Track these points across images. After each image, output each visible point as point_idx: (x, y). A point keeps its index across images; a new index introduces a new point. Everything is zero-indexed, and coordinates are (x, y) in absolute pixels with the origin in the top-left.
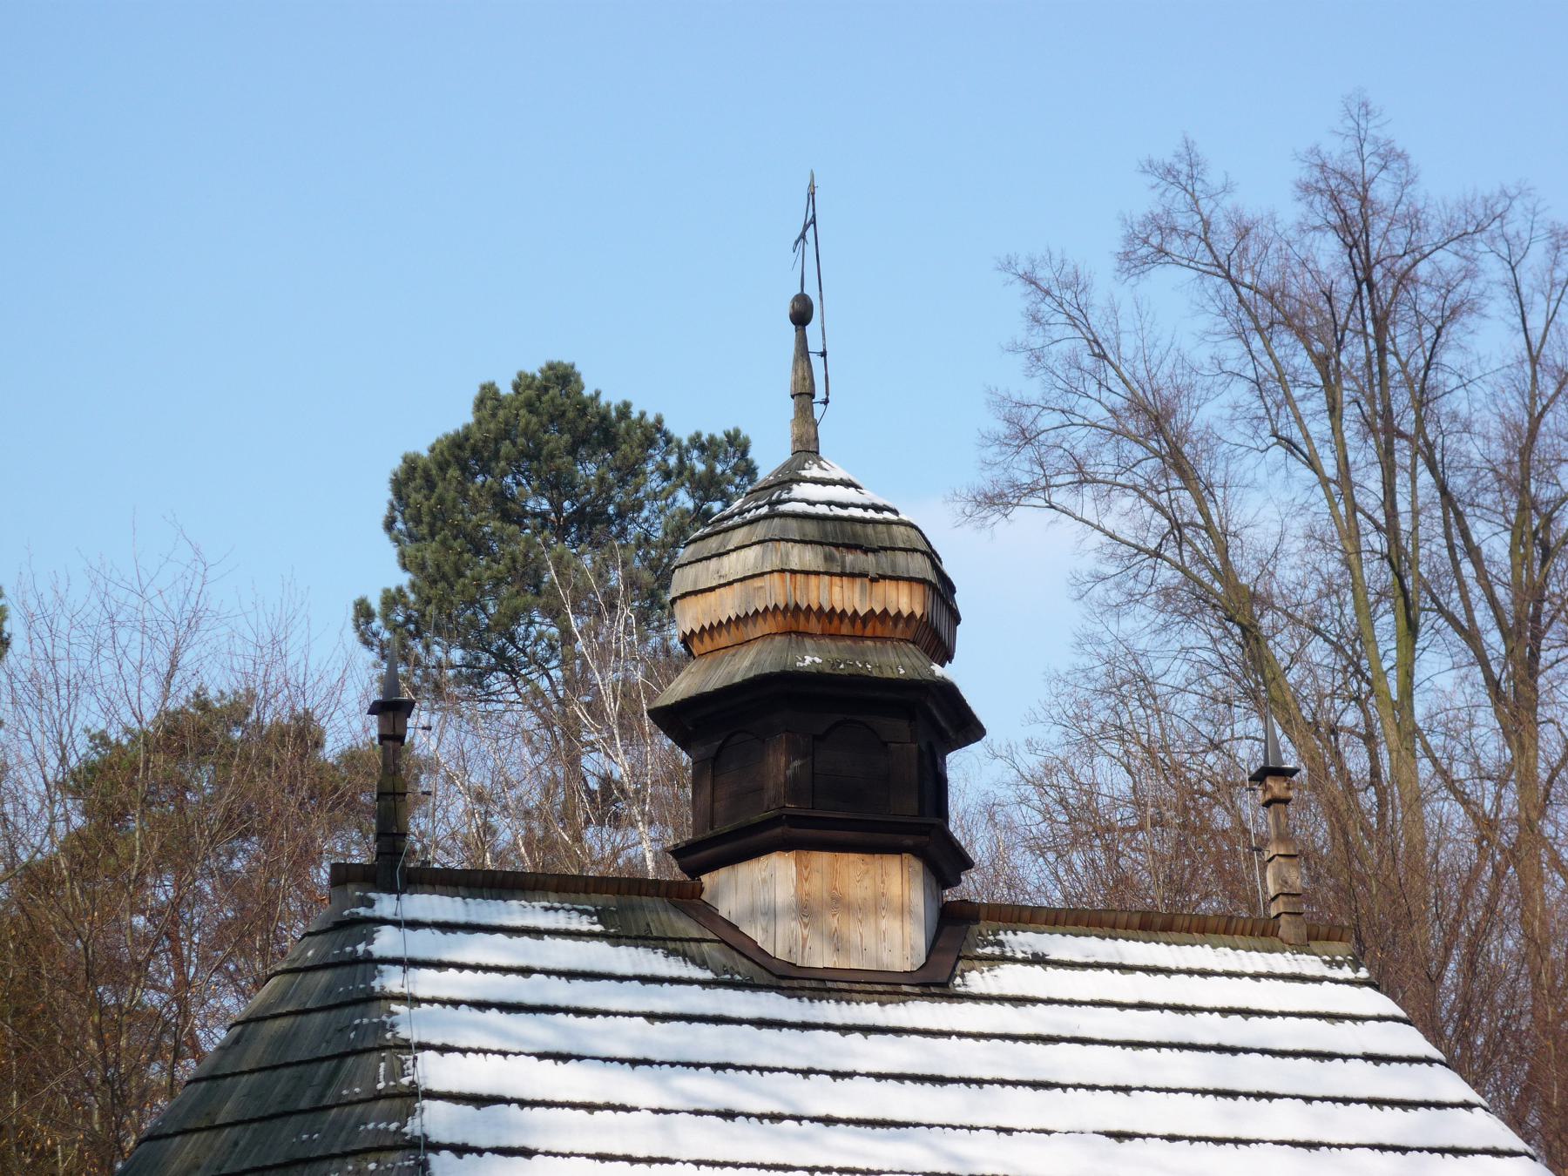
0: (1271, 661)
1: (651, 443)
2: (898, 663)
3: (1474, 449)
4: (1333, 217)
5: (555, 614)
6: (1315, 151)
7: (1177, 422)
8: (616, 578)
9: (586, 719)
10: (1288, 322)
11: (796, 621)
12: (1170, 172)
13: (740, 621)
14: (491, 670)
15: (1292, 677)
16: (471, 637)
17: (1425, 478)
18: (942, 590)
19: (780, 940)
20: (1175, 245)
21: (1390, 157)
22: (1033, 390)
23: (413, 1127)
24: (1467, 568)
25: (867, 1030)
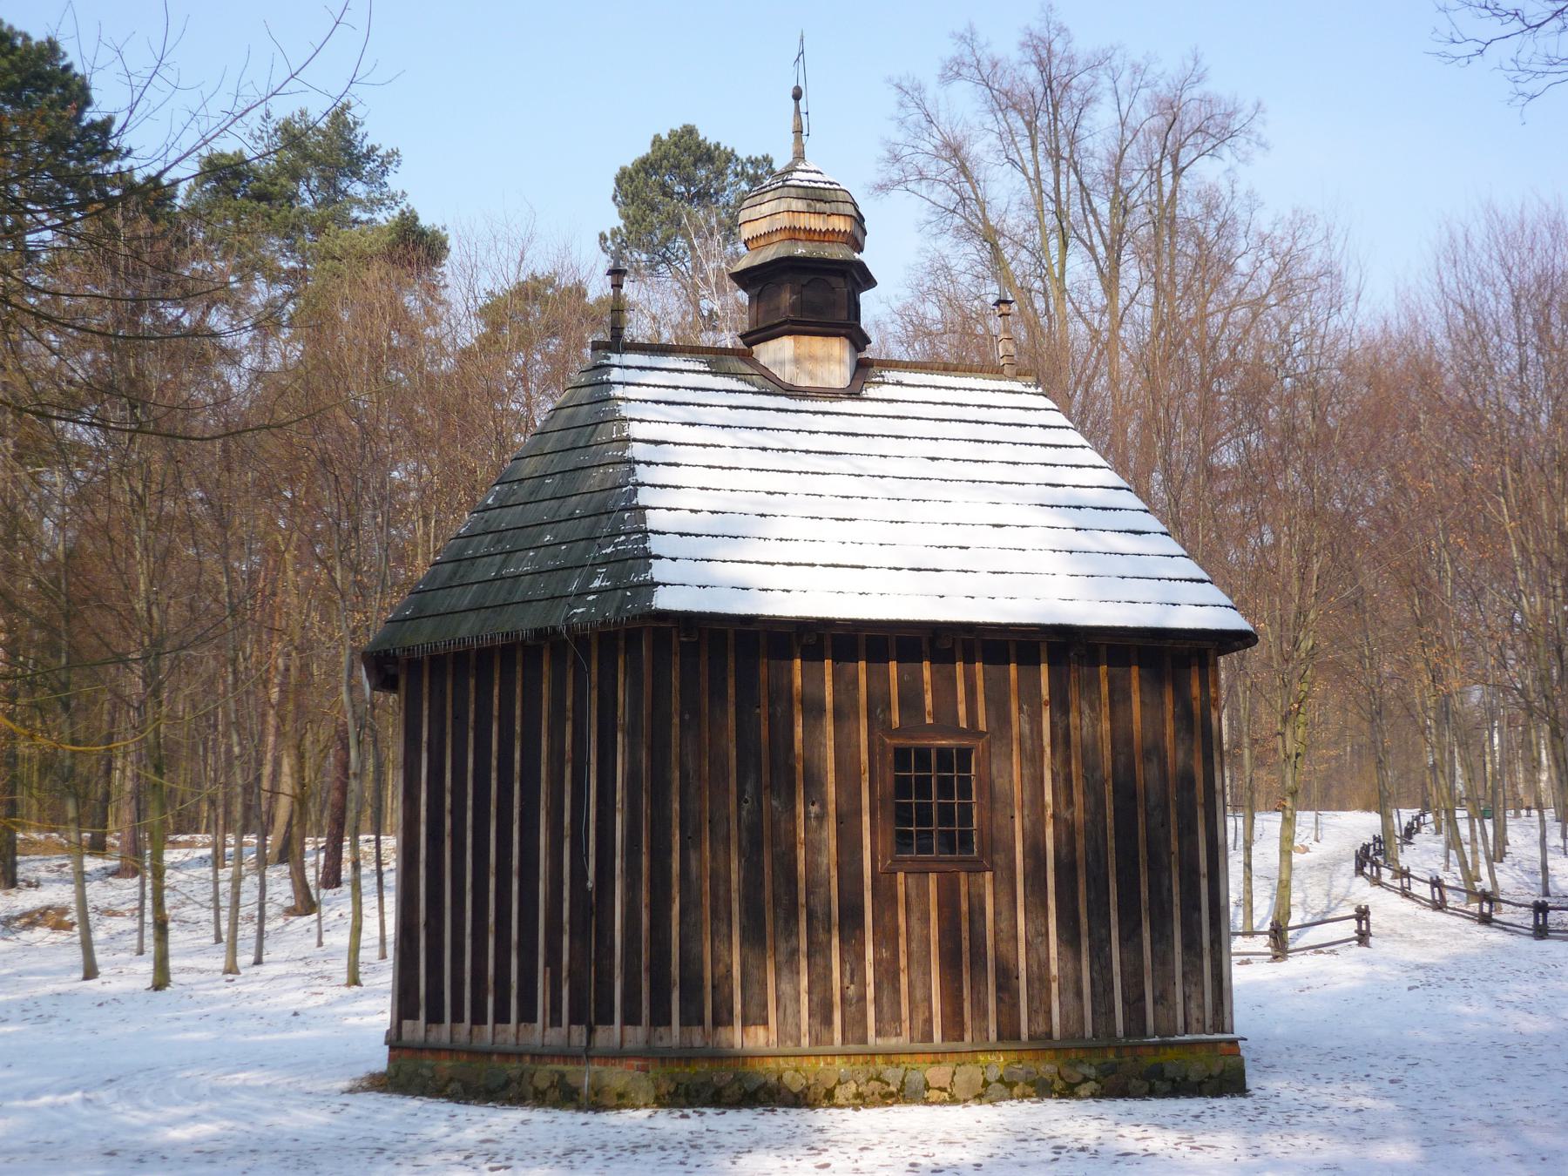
0: (1003, 260)
1: (729, 161)
2: (838, 252)
3: (1095, 165)
4: (1035, 58)
5: (686, 236)
6: (1028, 28)
7: (963, 153)
8: (713, 221)
9: (701, 284)
10: (1014, 106)
11: (793, 234)
12: (962, 37)
13: (769, 234)
14: (658, 263)
15: (1012, 267)
16: (650, 248)
17: (1073, 177)
18: (859, 220)
19: (787, 374)
20: (964, 71)
21: (1061, 30)
22: (899, 137)
23: (628, 454)
24: (1090, 218)
25: (824, 413)
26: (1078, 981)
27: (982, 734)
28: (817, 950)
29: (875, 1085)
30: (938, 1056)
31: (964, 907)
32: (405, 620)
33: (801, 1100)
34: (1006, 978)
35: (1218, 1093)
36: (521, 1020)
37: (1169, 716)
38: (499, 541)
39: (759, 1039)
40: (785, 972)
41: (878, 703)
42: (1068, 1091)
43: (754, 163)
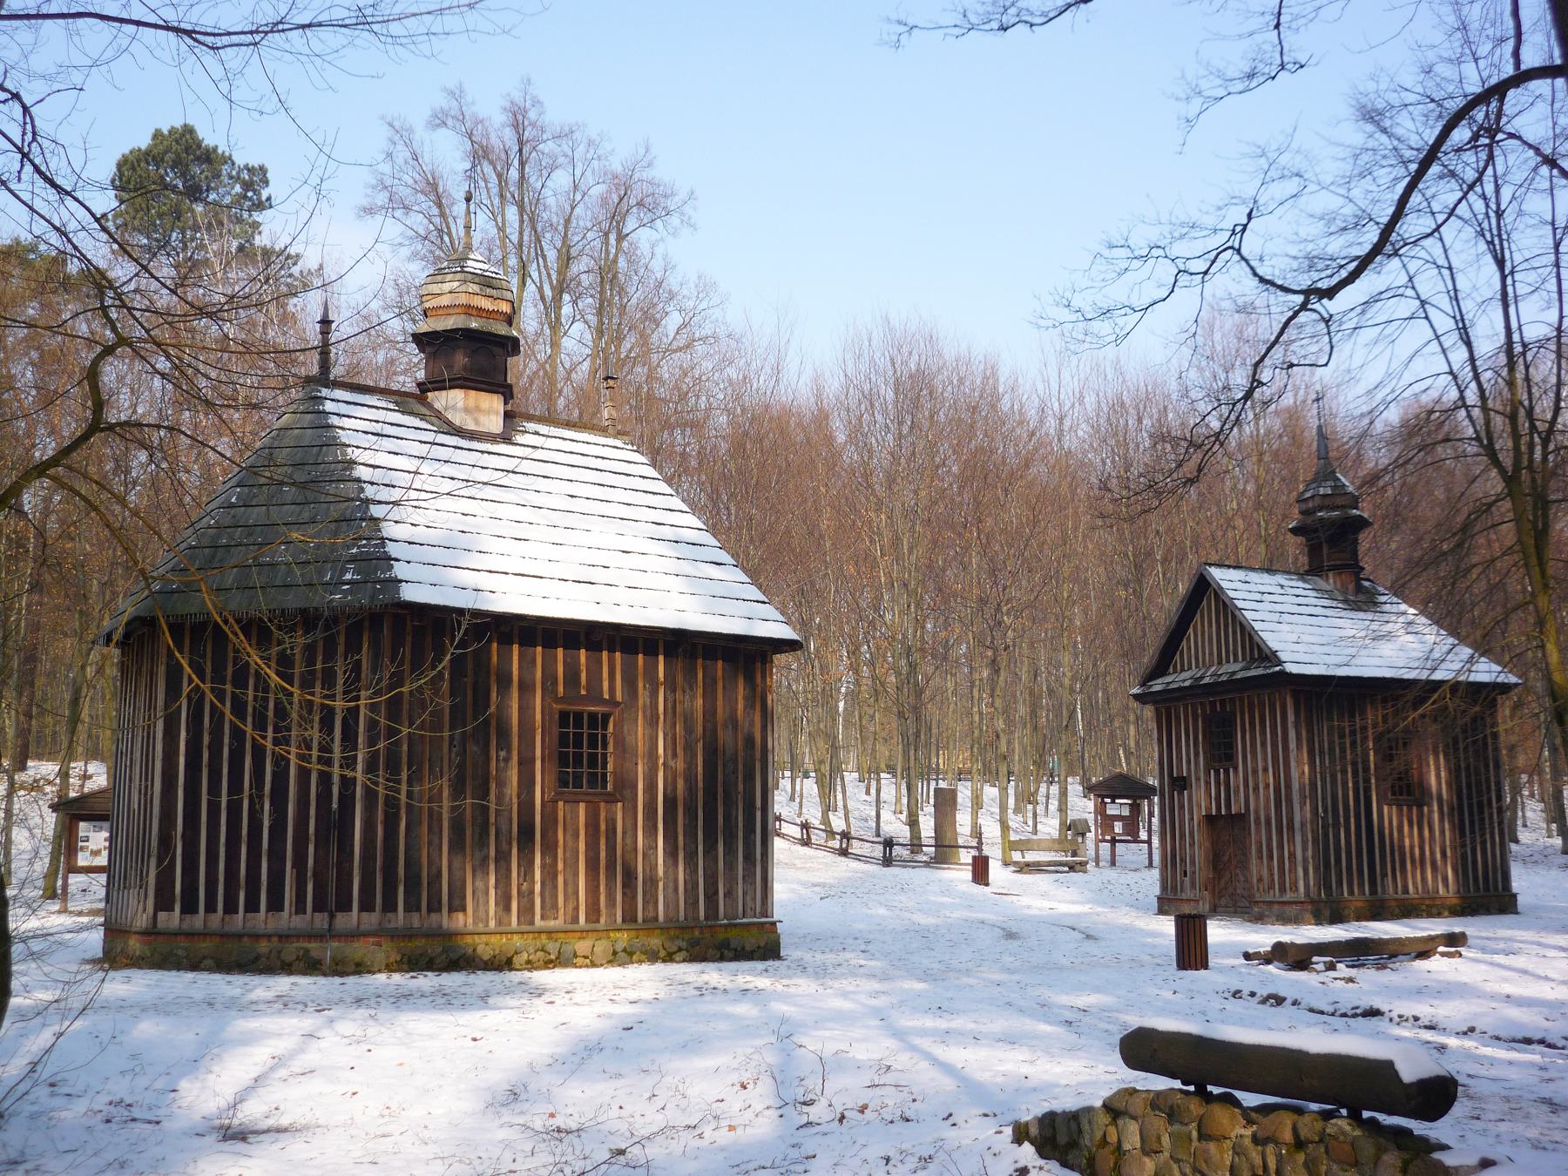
2: (501, 329)
11: (469, 310)
12: (452, 93)
19: (457, 419)
20: (450, 122)
21: (536, 102)
26: (676, 881)
27: (618, 704)
28: (502, 858)
29: (540, 954)
30: (584, 933)
31: (603, 827)
32: (173, 592)
33: (502, 964)
34: (629, 876)
35: (764, 958)
36: (226, 911)
37: (740, 697)
38: (250, 535)
39: (461, 921)
40: (479, 874)
41: (549, 678)
42: (669, 958)
43: (251, 170)
